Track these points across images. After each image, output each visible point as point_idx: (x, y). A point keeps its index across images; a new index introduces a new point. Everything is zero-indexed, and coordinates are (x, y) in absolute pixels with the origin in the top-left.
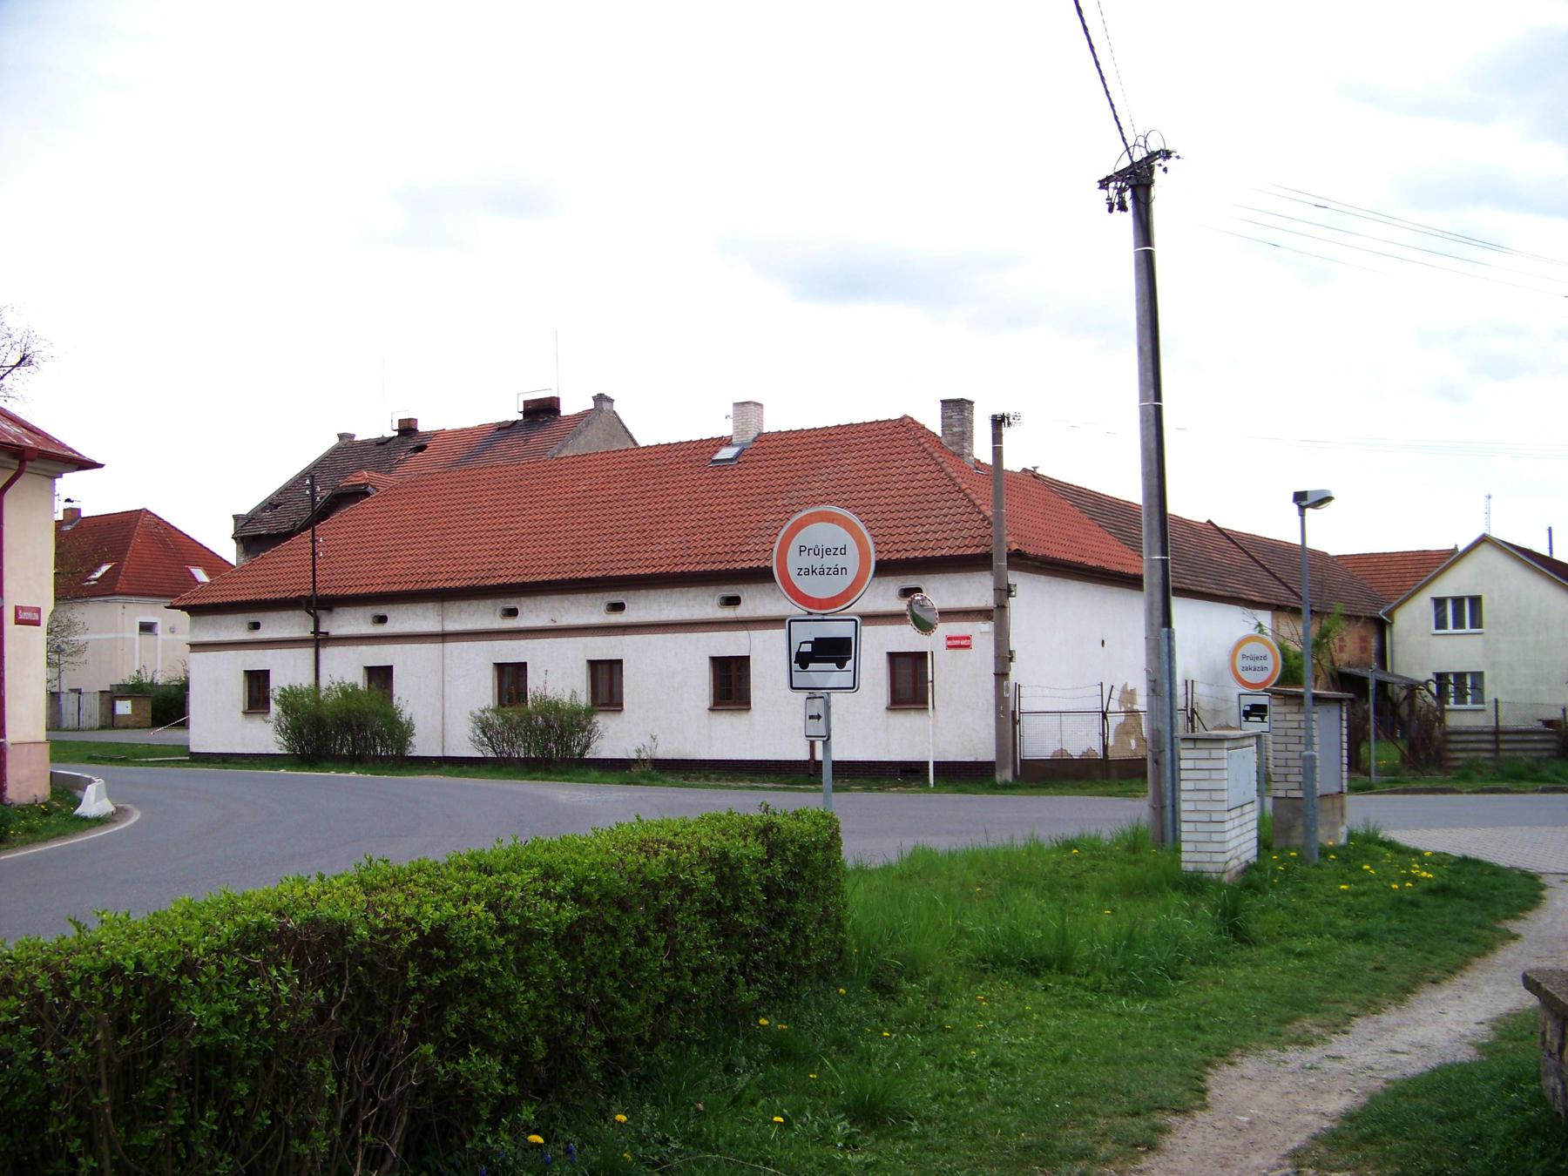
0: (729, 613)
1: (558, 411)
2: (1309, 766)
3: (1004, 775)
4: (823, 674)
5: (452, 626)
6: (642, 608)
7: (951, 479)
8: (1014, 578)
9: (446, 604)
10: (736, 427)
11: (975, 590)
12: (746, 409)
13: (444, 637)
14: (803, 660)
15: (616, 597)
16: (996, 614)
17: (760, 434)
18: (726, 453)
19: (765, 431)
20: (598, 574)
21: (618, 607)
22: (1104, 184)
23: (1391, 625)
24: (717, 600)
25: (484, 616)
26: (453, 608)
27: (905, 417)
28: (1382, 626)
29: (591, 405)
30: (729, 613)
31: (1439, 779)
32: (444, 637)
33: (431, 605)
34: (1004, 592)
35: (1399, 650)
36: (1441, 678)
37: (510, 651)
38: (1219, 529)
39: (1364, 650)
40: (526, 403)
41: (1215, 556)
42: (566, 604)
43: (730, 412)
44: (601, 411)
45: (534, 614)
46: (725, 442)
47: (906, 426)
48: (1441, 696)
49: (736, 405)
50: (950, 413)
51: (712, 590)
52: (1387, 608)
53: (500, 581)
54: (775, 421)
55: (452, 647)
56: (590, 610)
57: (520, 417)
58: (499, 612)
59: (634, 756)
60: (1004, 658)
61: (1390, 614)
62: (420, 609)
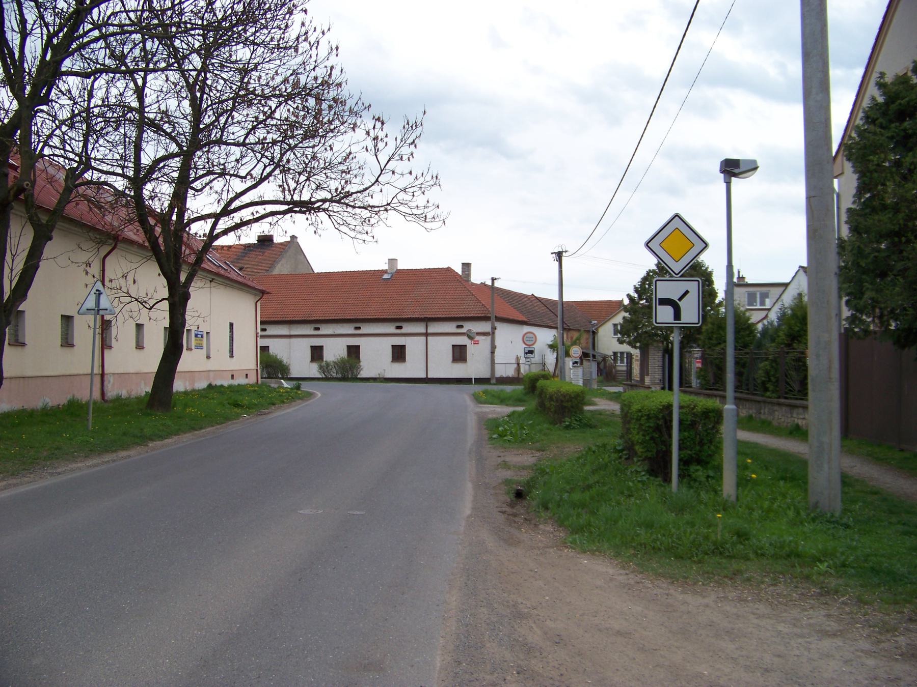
0: (398, 331)
1: (272, 240)
2: (591, 373)
3: (494, 381)
4: (529, 355)
5: (293, 333)
6: (366, 329)
7: (469, 291)
8: (497, 324)
9: (291, 325)
10: (389, 267)
11: (485, 327)
12: (392, 261)
13: (290, 336)
14: (526, 353)
15: (358, 325)
16: (492, 334)
17: (397, 270)
18: (386, 276)
19: (398, 268)
20: (353, 317)
21: (359, 328)
22: (552, 253)
23: (597, 333)
24: (394, 327)
25: (308, 330)
26: (294, 327)
27: (449, 268)
28: (594, 333)
29: (289, 239)
30: (398, 331)
31: (614, 383)
32: (290, 336)
33: (285, 326)
34: (494, 328)
35: (600, 343)
36: (615, 354)
37: (317, 342)
38: (536, 298)
39: (587, 343)
40: (259, 236)
41: (537, 309)
42: (339, 327)
43: (387, 262)
44: (294, 242)
45: (326, 329)
46: (384, 272)
47: (449, 270)
48: (615, 360)
49: (389, 259)
50: (464, 267)
51: (393, 324)
52: (596, 327)
53: (315, 318)
54: (401, 266)
55: (293, 340)
56: (348, 329)
57: (256, 242)
58: (312, 329)
59: (378, 377)
60: (493, 348)
61: (597, 329)
62: (280, 327)
